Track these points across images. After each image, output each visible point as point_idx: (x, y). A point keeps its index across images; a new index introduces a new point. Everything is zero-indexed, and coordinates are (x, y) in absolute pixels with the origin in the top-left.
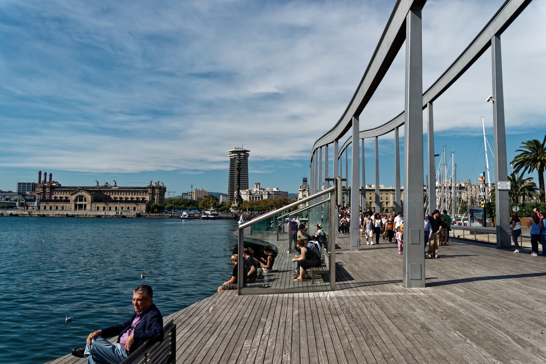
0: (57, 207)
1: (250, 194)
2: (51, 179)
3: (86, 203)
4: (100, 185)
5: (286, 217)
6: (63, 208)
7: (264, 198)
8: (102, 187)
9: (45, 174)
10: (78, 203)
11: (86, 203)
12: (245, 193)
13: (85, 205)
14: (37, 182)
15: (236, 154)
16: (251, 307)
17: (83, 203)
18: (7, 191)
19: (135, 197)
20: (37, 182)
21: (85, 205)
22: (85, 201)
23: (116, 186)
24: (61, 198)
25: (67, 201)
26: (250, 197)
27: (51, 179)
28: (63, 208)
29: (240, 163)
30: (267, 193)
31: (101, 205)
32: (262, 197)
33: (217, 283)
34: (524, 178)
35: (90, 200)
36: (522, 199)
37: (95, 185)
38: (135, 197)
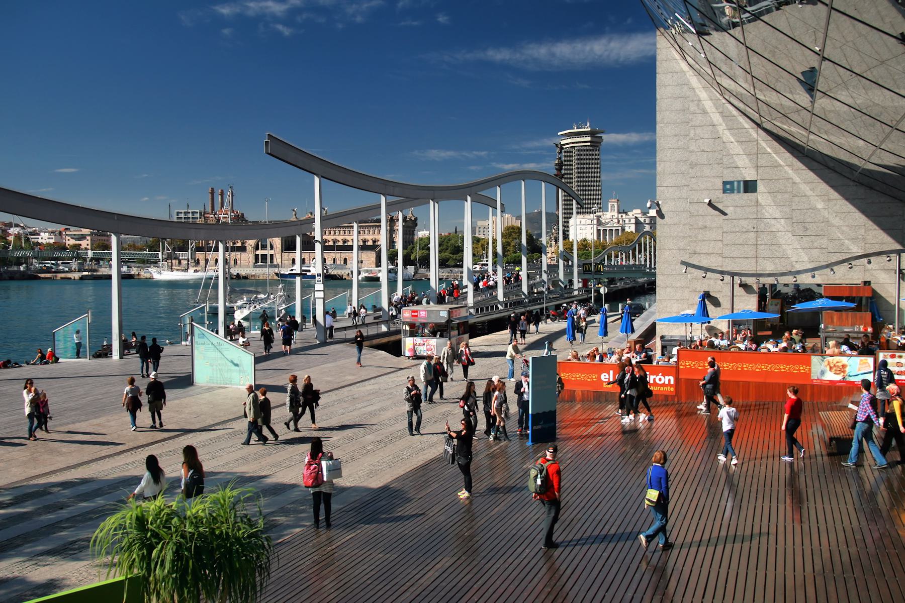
1: (599, 223)
3: (272, 252)
5: (266, 300)
7: (627, 229)
10: (260, 252)
11: (272, 252)
12: (589, 222)
13: (272, 256)
15: (589, 139)
16: (322, 574)
17: (268, 252)
21: (272, 256)
22: (272, 248)
24: (335, 241)
26: (599, 231)
30: (633, 221)
32: (623, 229)
33: (94, 511)
35: (279, 246)
36: (579, 376)
38: (340, 238)
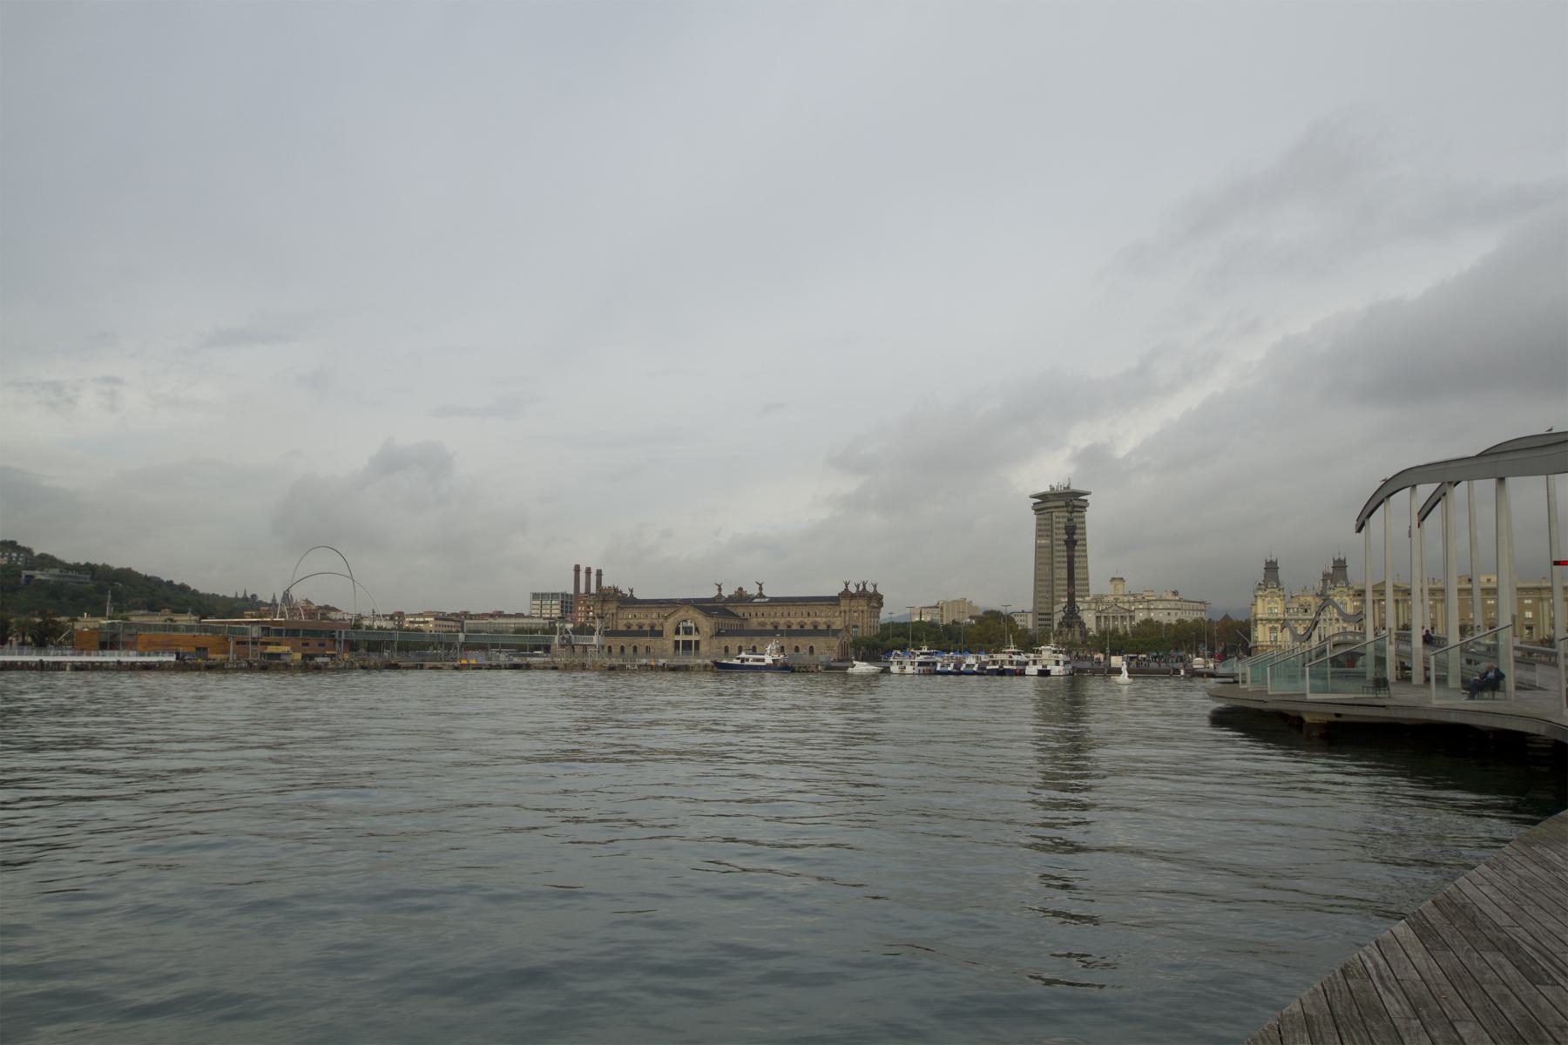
0: (635, 649)
2: (599, 582)
3: (677, 638)
4: (726, 593)
6: (648, 649)
8: (731, 599)
9: (588, 571)
13: (697, 643)
14: (571, 591)
17: (693, 638)
18: (834, 589)
19: (808, 621)
20: (571, 591)
21: (697, 643)
23: (761, 595)
25: (656, 633)
27: (599, 582)
28: (648, 649)
29: (1061, 511)
31: (733, 643)
34: (1481, 641)
37: (711, 593)
38: (808, 621)
